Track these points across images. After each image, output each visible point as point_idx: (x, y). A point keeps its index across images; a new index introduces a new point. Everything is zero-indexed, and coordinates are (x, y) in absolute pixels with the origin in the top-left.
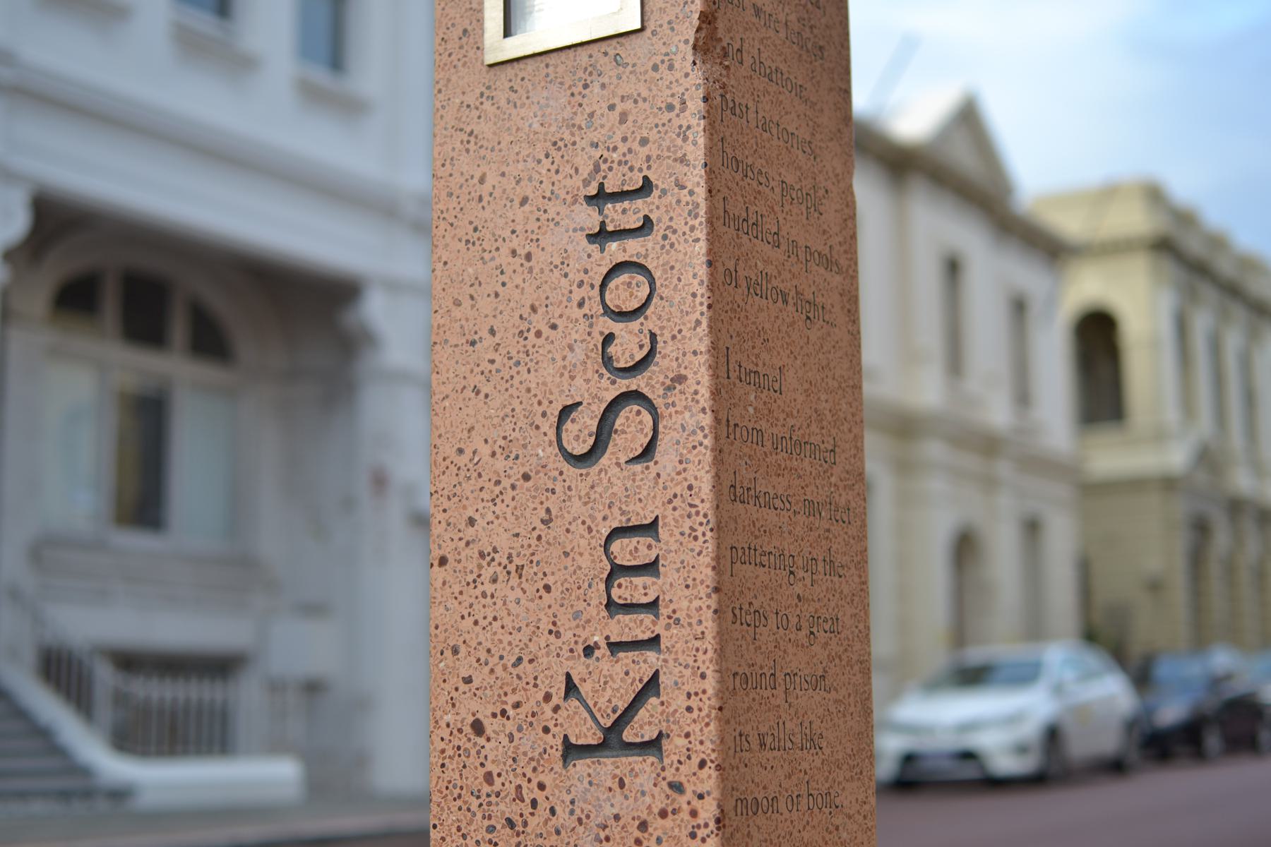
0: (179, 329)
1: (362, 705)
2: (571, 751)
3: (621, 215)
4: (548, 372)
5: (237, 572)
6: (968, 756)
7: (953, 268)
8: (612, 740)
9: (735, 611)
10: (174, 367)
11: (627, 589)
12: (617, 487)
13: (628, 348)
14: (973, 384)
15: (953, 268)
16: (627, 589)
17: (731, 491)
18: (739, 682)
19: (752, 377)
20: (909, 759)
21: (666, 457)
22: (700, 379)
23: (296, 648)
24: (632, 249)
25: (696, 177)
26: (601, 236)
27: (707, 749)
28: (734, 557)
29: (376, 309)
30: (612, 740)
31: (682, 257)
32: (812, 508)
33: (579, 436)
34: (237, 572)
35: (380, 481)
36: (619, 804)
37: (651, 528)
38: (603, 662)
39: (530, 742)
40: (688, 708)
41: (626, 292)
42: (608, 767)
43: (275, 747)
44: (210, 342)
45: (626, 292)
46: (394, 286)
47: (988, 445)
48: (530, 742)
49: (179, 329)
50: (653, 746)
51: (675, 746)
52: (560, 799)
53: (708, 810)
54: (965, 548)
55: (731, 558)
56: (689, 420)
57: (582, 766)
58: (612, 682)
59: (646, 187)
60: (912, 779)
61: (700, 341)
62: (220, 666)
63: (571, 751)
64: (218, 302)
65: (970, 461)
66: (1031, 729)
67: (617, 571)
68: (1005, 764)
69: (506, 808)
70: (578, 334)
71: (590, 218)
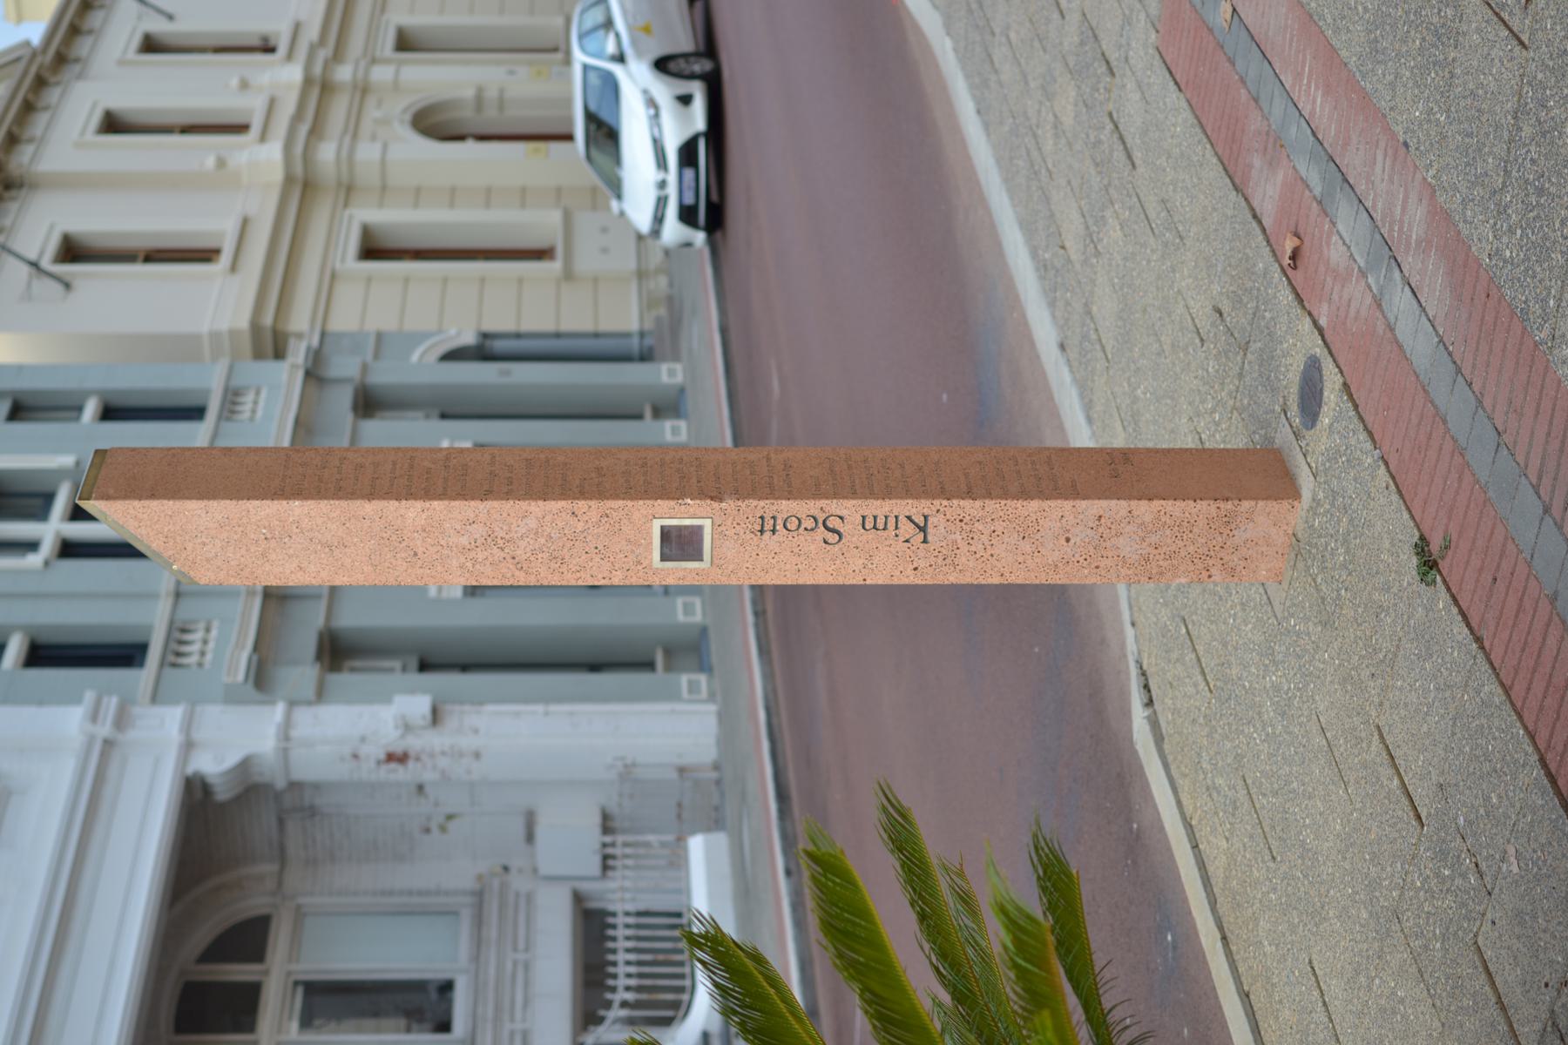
0: (239, 972)
1: (628, 773)
2: (925, 541)
3: (769, 525)
4: (812, 547)
5: (487, 906)
6: (688, 154)
7: (113, 124)
8: (923, 529)
9: (887, 494)
10: (277, 977)
11: (880, 525)
12: (850, 528)
13: (809, 523)
14: (252, 106)
15: (113, 124)
16: (880, 525)
17: (854, 494)
18: (908, 493)
19: (818, 486)
20: (687, 215)
21: (844, 513)
22: (823, 503)
23: (568, 844)
24: (780, 522)
25: (762, 503)
26: (774, 531)
27: (928, 502)
28: (871, 493)
29: (212, 764)
30: (923, 529)
31: (786, 507)
32: (850, 467)
33: (832, 538)
34: (487, 906)
35: (396, 758)
36: (941, 527)
37: (864, 518)
38: (900, 531)
39: (921, 554)
40: (915, 508)
41: (793, 524)
42: (930, 530)
43: (678, 860)
44: (248, 939)
45: (793, 524)
46: (188, 746)
47: (319, 88)
48: (921, 554)
49: (239, 972)
50: (926, 517)
51: (926, 511)
52: (939, 544)
53: (945, 502)
54: (435, 124)
55: (872, 495)
56: (834, 506)
57: (929, 538)
58: (907, 529)
59: (762, 518)
60: (709, 214)
61: (811, 503)
62: (592, 925)
63: (925, 541)
64: (203, 935)
65: (339, 110)
66: (663, 90)
67: (875, 527)
68: (698, 118)
69: (940, 560)
70: (802, 538)
71: (767, 534)
